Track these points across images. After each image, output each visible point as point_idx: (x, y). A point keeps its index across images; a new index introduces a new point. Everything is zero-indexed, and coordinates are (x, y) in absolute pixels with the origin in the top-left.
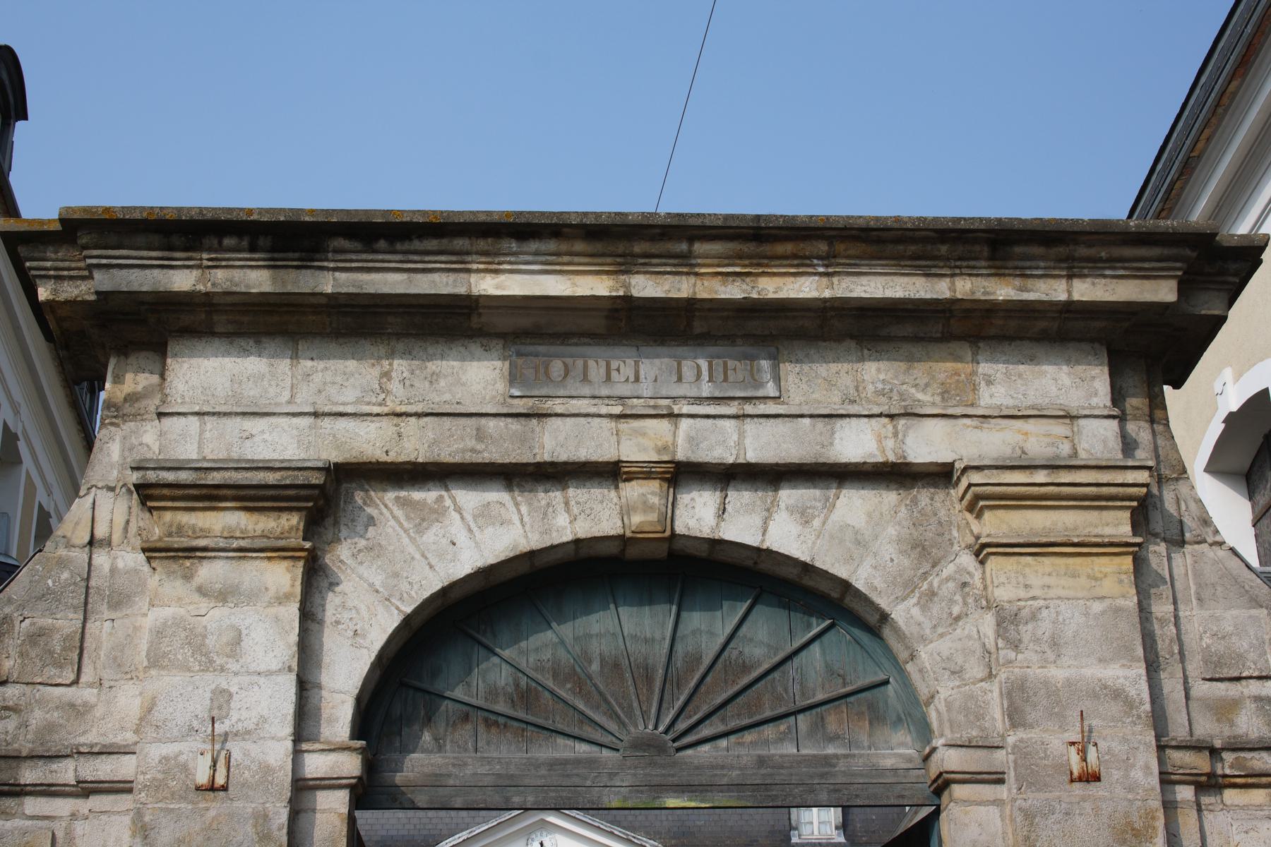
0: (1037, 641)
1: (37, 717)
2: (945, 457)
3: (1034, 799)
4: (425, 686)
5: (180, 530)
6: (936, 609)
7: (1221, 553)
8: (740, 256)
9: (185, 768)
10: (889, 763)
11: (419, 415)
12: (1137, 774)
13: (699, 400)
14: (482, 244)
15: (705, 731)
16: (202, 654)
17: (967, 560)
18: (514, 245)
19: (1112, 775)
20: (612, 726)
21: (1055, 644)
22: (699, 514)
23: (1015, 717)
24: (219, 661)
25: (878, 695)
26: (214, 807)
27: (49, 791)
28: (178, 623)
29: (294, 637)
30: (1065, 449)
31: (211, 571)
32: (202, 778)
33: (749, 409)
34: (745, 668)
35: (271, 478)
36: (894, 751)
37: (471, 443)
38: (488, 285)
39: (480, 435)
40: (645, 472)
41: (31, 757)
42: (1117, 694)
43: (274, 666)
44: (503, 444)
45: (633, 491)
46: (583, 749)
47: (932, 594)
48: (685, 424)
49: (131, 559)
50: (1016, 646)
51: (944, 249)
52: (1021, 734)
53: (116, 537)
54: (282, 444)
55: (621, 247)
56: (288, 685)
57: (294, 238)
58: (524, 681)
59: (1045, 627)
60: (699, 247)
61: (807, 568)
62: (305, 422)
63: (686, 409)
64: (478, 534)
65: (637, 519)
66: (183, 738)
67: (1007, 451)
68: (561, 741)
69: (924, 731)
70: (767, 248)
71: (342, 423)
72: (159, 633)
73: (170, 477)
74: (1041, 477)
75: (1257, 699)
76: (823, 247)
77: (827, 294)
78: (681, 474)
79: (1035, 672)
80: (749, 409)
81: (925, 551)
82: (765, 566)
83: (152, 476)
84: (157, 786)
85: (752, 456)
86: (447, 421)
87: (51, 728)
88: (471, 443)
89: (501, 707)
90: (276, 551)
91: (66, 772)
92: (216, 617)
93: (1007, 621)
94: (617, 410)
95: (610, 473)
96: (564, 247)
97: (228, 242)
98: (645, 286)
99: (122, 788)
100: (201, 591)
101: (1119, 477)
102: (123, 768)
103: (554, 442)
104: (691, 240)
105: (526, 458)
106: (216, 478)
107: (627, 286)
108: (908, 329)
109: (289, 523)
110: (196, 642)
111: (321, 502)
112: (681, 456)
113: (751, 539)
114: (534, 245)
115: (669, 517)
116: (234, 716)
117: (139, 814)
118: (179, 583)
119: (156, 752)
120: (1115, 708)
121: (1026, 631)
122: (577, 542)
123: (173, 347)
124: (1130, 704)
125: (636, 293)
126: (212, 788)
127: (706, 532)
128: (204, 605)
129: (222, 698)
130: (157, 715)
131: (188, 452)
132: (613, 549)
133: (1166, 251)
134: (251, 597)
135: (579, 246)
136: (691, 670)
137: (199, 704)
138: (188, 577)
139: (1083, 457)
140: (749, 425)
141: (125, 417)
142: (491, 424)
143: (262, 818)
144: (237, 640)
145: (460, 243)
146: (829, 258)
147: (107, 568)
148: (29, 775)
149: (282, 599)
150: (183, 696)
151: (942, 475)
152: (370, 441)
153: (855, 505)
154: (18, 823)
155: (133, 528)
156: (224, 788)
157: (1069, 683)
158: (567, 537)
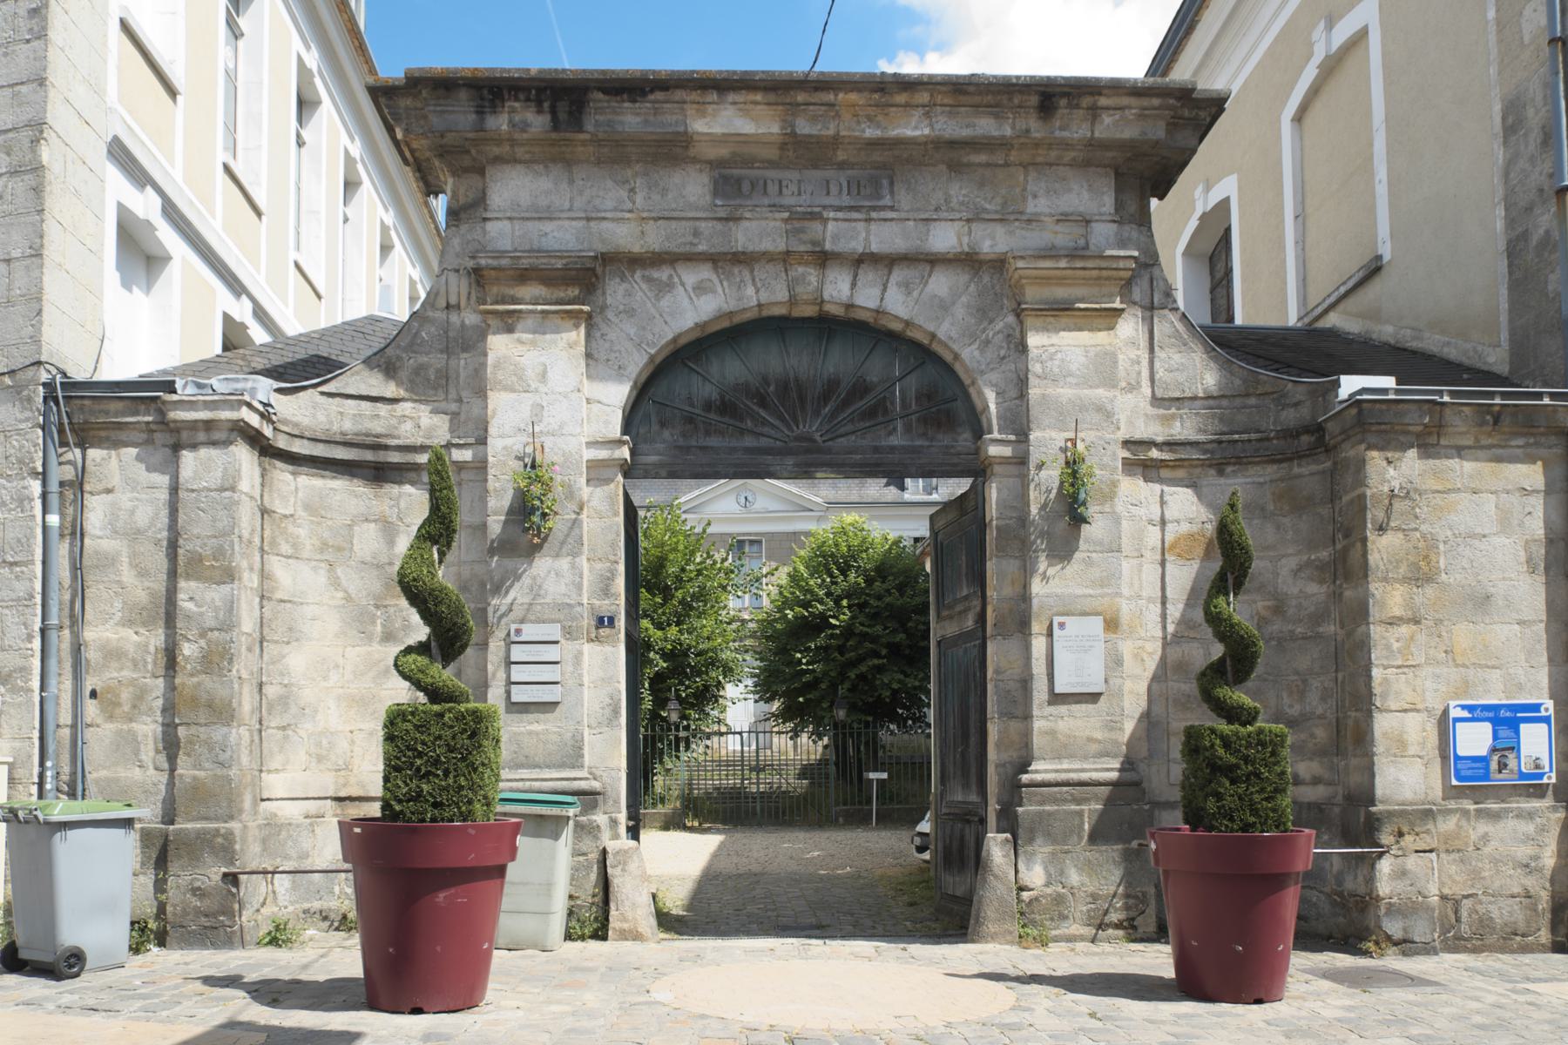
15: (842, 430)
22: (838, 289)
44: (710, 238)
49: (471, 318)
53: (463, 304)
54: (563, 237)
64: (693, 303)
107: (793, 126)
137: (526, 412)
152: (623, 236)
153: (941, 283)
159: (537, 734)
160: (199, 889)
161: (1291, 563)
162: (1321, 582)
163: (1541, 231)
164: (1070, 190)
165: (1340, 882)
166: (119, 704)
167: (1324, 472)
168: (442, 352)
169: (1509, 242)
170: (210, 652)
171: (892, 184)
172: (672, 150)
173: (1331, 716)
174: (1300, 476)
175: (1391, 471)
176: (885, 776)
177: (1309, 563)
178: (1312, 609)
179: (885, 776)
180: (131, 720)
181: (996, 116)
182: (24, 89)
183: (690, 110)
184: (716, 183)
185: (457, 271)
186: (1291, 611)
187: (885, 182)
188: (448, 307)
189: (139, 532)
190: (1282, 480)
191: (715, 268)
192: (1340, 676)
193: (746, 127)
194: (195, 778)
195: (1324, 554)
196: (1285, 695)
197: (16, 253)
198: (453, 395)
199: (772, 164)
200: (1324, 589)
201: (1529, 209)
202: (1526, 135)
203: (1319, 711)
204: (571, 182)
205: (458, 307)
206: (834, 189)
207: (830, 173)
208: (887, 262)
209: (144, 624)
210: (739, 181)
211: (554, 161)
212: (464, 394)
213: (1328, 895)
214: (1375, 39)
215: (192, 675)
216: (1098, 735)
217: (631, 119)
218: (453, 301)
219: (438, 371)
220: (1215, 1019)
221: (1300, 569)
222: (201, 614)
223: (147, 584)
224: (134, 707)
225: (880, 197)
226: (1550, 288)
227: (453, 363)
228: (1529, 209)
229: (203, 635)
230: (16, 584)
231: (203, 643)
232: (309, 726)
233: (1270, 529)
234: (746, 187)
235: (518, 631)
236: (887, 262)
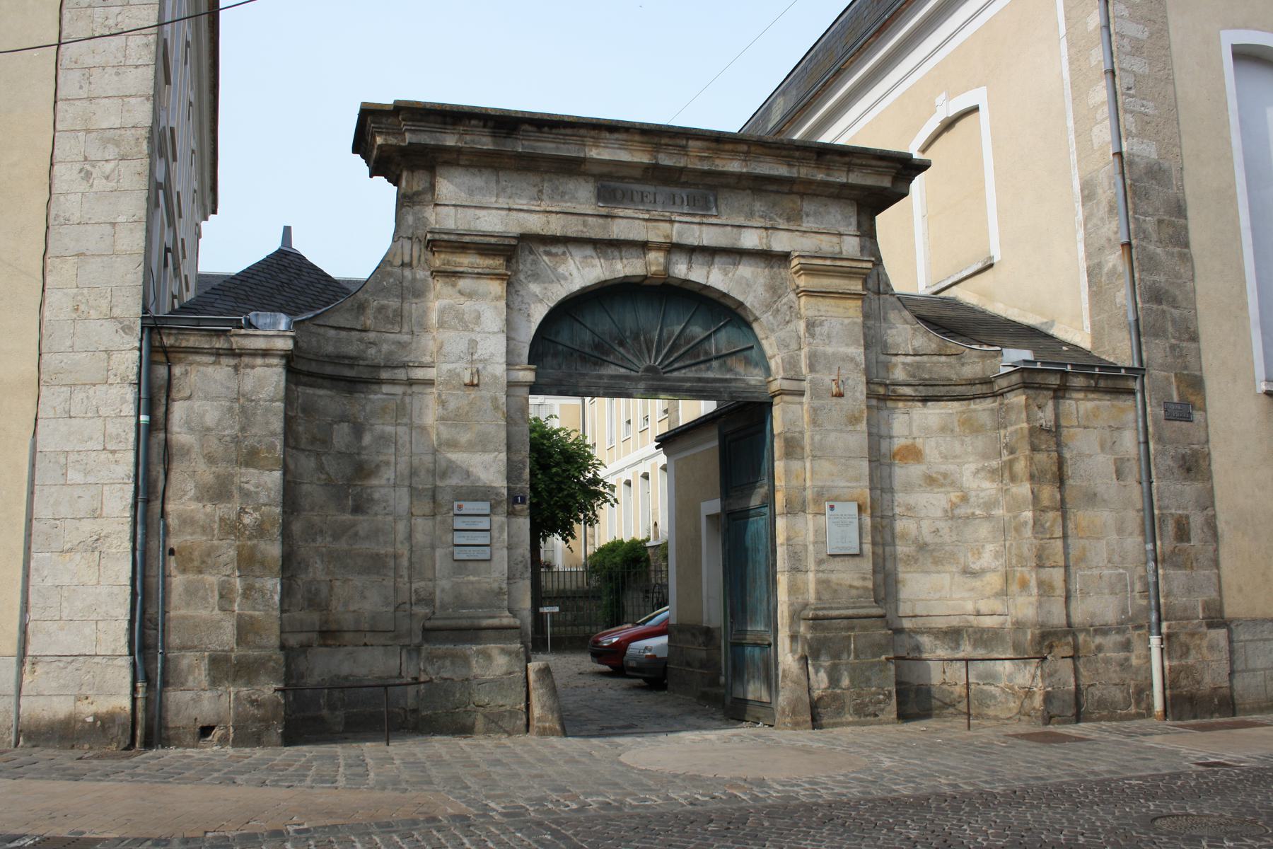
0: (821, 335)
1: (385, 348)
2: (787, 249)
3: (817, 403)
4: (552, 338)
5: (448, 263)
6: (779, 318)
7: (894, 299)
8: (708, 149)
9: (458, 375)
10: (753, 383)
11: (557, 213)
12: (858, 394)
13: (682, 214)
14: (593, 133)
15: (676, 365)
16: (465, 323)
17: (792, 296)
18: (608, 135)
19: (848, 394)
20: (635, 361)
21: (829, 336)
22: (681, 269)
23: (812, 368)
24: (471, 326)
25: (751, 353)
26: (473, 393)
27: (393, 382)
28: (451, 307)
29: (504, 317)
30: (837, 249)
31: (463, 283)
32: (467, 380)
33: (705, 220)
34: (693, 338)
35: (493, 240)
36: (754, 377)
37: (581, 228)
38: (594, 153)
39: (585, 224)
40: (659, 247)
41: (386, 367)
42: (852, 360)
43: (496, 329)
44: (595, 229)
45: (652, 256)
46: (622, 371)
47: (778, 311)
48: (676, 225)
49: (421, 274)
50: (813, 336)
51: (797, 154)
52: (814, 375)
53: (415, 262)
54: (493, 221)
55: (656, 140)
56: (502, 339)
57: (505, 124)
58: (596, 339)
59: (825, 329)
60: (691, 143)
61: (725, 295)
62: (504, 213)
63: (678, 218)
64: (581, 272)
65: (653, 269)
66: (457, 361)
67: (813, 248)
68: (613, 367)
69: (768, 370)
70: (721, 146)
71: (521, 215)
72: (442, 312)
73: (445, 237)
74: (828, 262)
75: (904, 364)
76: (745, 148)
77: (744, 170)
78: (672, 248)
79: (821, 348)
80: (705, 220)
81: (775, 291)
82: (705, 292)
83: (437, 237)
84: (446, 383)
85: (705, 243)
86: (570, 217)
87: (391, 353)
88: (581, 228)
89: (587, 350)
90: (499, 277)
91: (401, 374)
92: (468, 305)
93: (811, 325)
94: (647, 216)
95: (644, 246)
96: (630, 137)
97: (473, 122)
98: (665, 160)
99: (430, 383)
100: (461, 293)
101: (860, 265)
102: (430, 374)
103: (620, 229)
104: (688, 139)
105: (606, 237)
106: (467, 239)
107: (656, 158)
108: (774, 188)
109: (496, 263)
110: (460, 316)
111: (510, 254)
112: (674, 240)
113: (702, 281)
114: (616, 136)
115: (666, 269)
116: (479, 352)
117: (440, 395)
118: (450, 288)
119: (445, 367)
120: (851, 366)
121: (818, 330)
122: (626, 277)
123: (439, 170)
124: (857, 365)
125: (661, 162)
126: (472, 385)
127: (682, 277)
128: (462, 299)
129: (473, 344)
130: (444, 351)
131: (450, 224)
132: (638, 280)
133: (890, 164)
134: (484, 296)
135: (637, 138)
136: (669, 338)
137: (463, 346)
138: (454, 286)
139: (845, 255)
140: (705, 228)
141: (414, 204)
142: (590, 219)
143: (494, 400)
144: (479, 317)
145: (583, 132)
146: (747, 153)
147: (410, 277)
148: (384, 375)
149: (498, 298)
150: (455, 342)
151: (785, 257)
152: (535, 224)
153: (746, 270)
154: (379, 396)
155: (423, 258)
156: (477, 385)
157: (833, 354)
158: (622, 275)
159: (472, 583)
160: (256, 701)
161: (972, 467)
162: (994, 481)
163: (1110, 265)
164: (829, 213)
165: (1010, 680)
166: (192, 560)
167: (992, 410)
168: (397, 296)
169: (1088, 268)
170: (263, 522)
171: (716, 200)
172: (572, 167)
173: (1002, 570)
174: (975, 411)
175: (1041, 414)
176: (556, 609)
177: (983, 468)
178: (986, 499)
179: (556, 609)
180: (200, 572)
181: (789, 165)
182: (133, 101)
183: (589, 141)
184: (599, 190)
185: (410, 239)
186: (972, 500)
187: (712, 199)
188: (403, 265)
189: (208, 429)
190: (963, 412)
191: (595, 248)
192: (1007, 544)
193: (624, 156)
194: (251, 617)
195: (994, 464)
196: (969, 555)
197: (121, 219)
198: (405, 329)
199: (637, 180)
200: (995, 485)
201: (1101, 249)
202: (1097, 204)
203: (993, 566)
204: (498, 182)
205: (410, 265)
206: (678, 200)
207: (676, 190)
208: (710, 253)
209: (211, 500)
210: (614, 190)
211: (485, 167)
212: (415, 329)
213: (1002, 689)
214: (984, 113)
215: (249, 539)
216: (856, 583)
217: (548, 147)
218: (407, 259)
219: (395, 311)
220: (1120, 738)
221: (978, 471)
222: (257, 493)
223: (213, 469)
224: (203, 562)
225: (709, 209)
226: (1118, 300)
227: (406, 306)
228: (1101, 249)
229: (255, 510)
230: (113, 466)
231: (257, 515)
232: (303, 576)
233: (957, 445)
234: (619, 195)
235: (460, 507)
236: (710, 253)
